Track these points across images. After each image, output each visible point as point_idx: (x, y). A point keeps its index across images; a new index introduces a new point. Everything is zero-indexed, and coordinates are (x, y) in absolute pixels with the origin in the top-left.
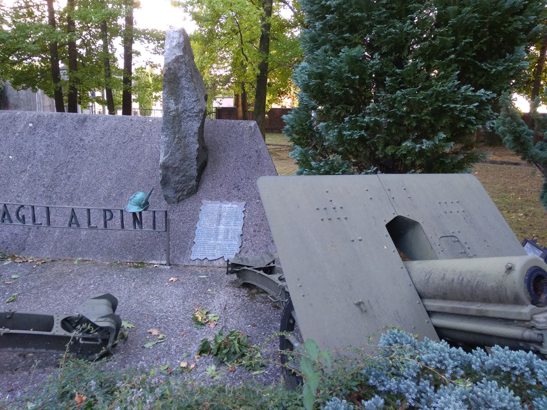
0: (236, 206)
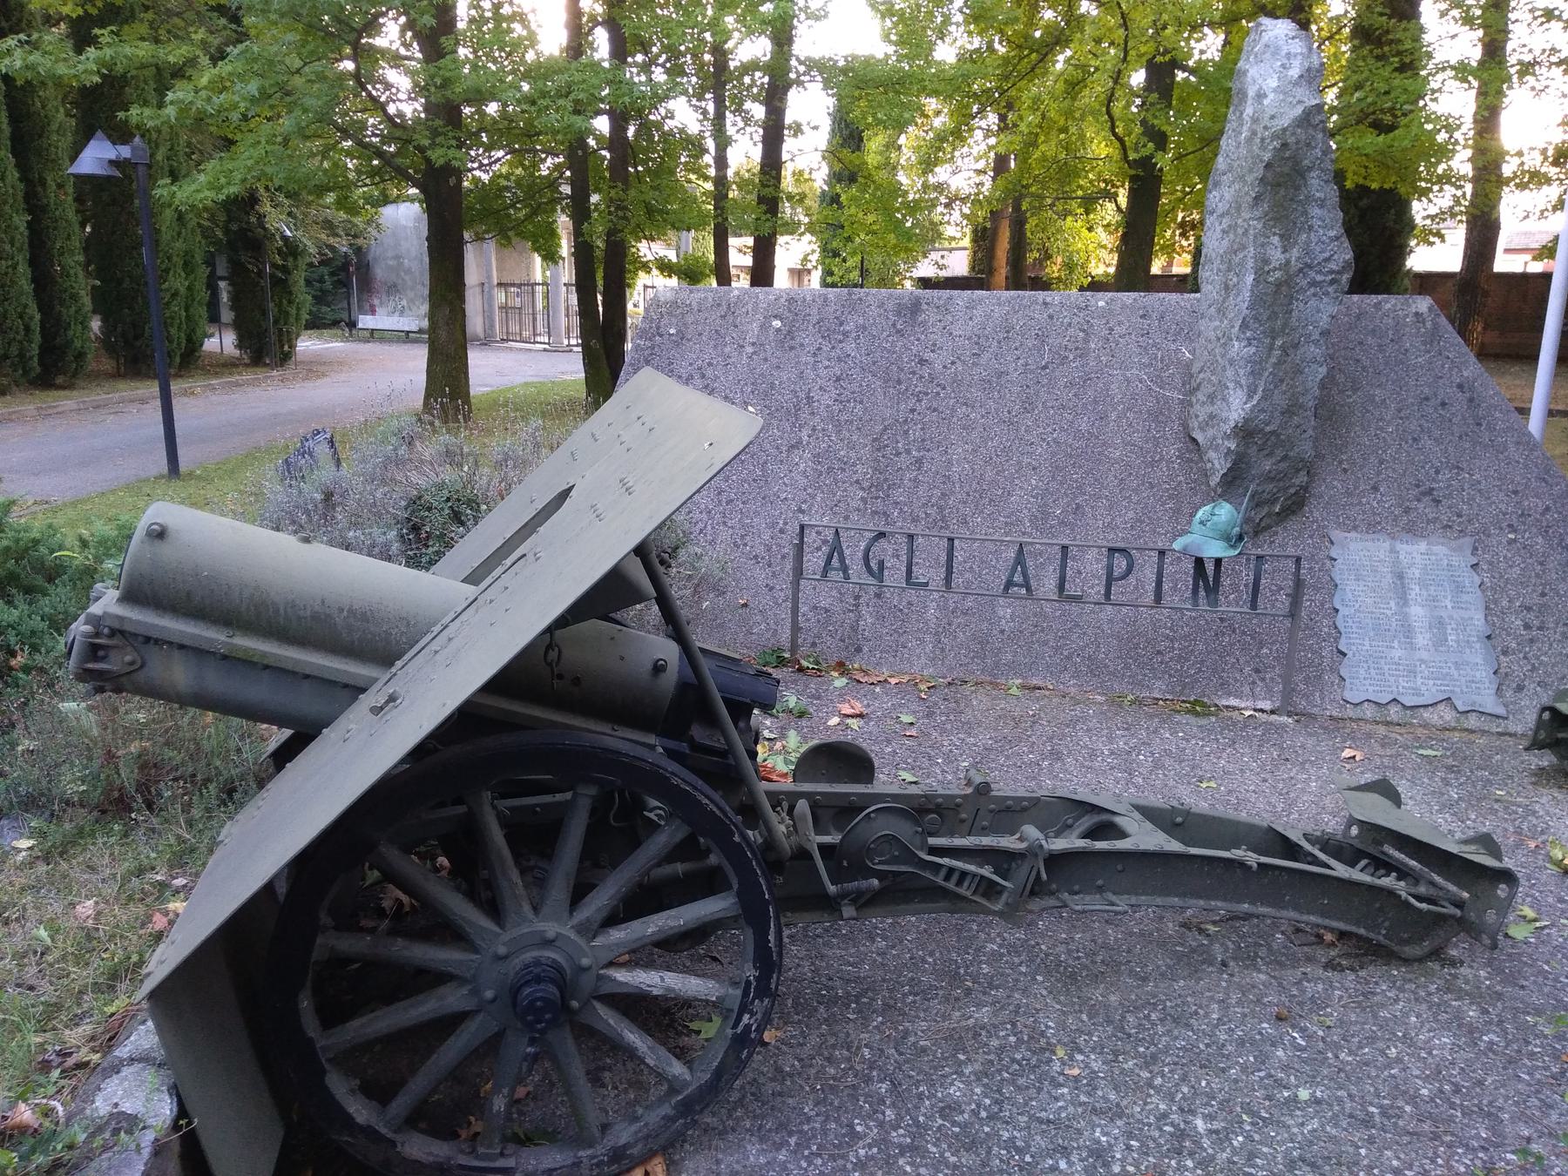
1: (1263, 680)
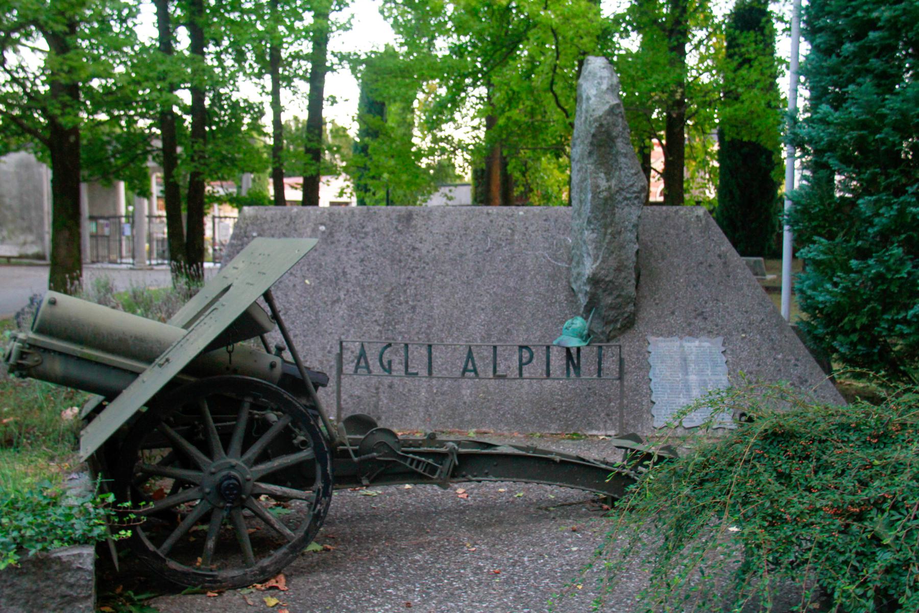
0: (706, 344)
1: (611, 419)
